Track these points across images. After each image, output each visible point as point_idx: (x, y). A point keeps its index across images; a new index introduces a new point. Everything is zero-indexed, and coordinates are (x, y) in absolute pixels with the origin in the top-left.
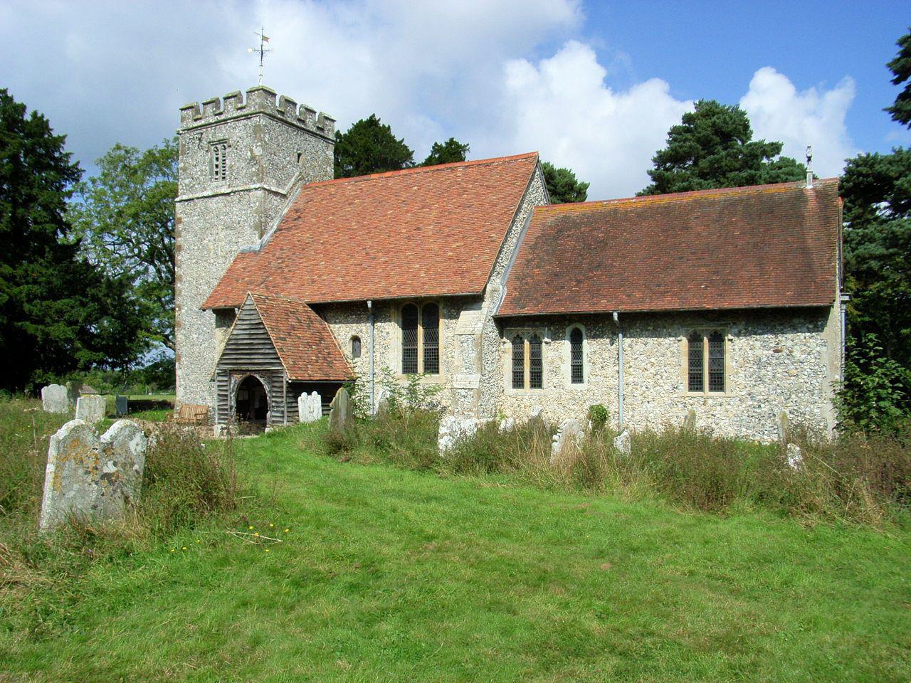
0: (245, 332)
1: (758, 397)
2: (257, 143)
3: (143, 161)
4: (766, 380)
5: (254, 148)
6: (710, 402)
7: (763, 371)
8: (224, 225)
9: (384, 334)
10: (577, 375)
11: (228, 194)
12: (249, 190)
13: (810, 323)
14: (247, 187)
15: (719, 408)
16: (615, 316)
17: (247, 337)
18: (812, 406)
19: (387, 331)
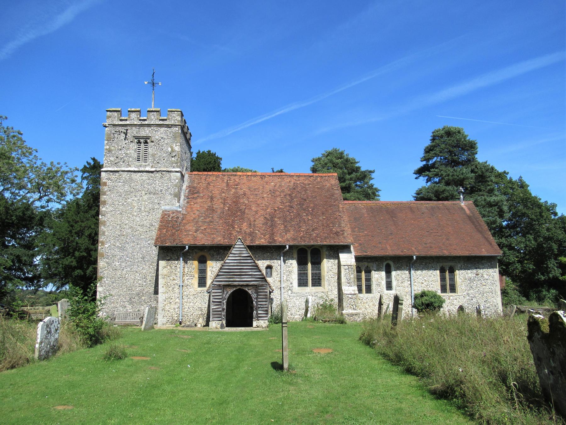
1: (471, 295)
3: (465, 141)
4: (474, 287)
6: (451, 298)
7: (472, 284)
11: (152, 172)
13: (489, 262)
15: (455, 301)
16: (415, 257)
18: (493, 299)
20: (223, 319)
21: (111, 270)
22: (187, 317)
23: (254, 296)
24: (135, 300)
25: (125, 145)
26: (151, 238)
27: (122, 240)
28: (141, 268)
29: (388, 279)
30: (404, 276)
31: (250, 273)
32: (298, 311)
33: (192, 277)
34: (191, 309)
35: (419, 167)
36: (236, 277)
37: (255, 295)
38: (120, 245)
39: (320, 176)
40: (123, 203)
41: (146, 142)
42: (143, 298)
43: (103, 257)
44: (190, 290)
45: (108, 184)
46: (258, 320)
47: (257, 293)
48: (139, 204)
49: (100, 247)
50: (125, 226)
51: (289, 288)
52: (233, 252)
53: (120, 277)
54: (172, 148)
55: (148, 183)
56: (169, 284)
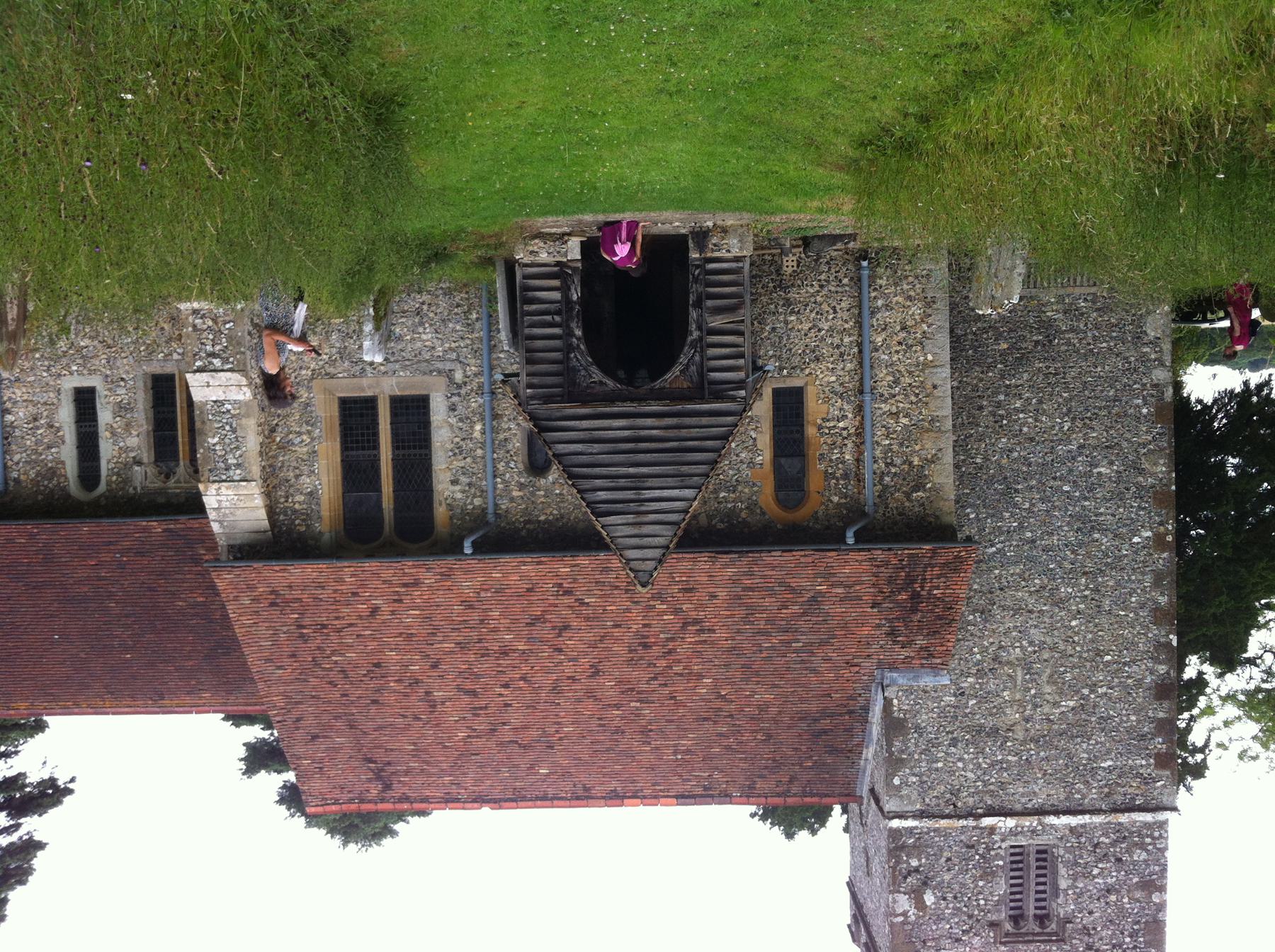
0: (657, 493)
2: (903, 923)
5: (912, 911)
8: (1006, 739)
9: (464, 480)
10: (85, 401)
11: (991, 812)
12: (921, 815)
14: (926, 823)
17: (651, 482)
19: (458, 488)
20: (697, 267)
21: (1125, 444)
22: (840, 275)
23: (581, 358)
24: (1035, 338)
25: (1091, 906)
26: (984, 566)
27: (1088, 555)
28: (1015, 454)
29: (88, 430)
30: (28, 442)
31: (597, 447)
32: (423, 303)
33: (828, 424)
34: (825, 307)
35: (36, 817)
36: (655, 432)
37: (574, 363)
38: (1096, 536)
39: (370, 802)
40: (1092, 691)
41: (1016, 919)
42: (1005, 346)
43: (1155, 493)
44: (833, 379)
45: (1152, 761)
46: (558, 264)
47: (568, 372)
48: (1033, 692)
49: (1170, 527)
50: (1082, 606)
51: (463, 391)
52: (667, 531)
53: (1090, 419)
54: (920, 905)
55: (1006, 770)
56: (913, 398)
